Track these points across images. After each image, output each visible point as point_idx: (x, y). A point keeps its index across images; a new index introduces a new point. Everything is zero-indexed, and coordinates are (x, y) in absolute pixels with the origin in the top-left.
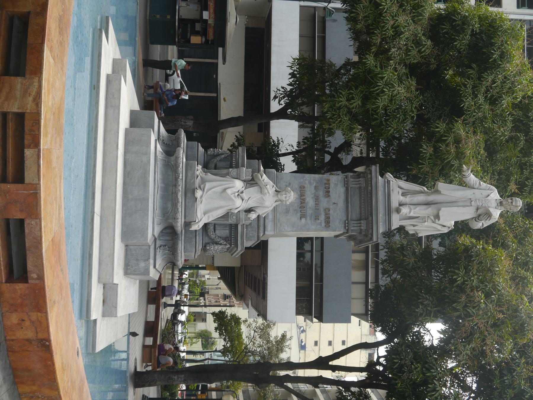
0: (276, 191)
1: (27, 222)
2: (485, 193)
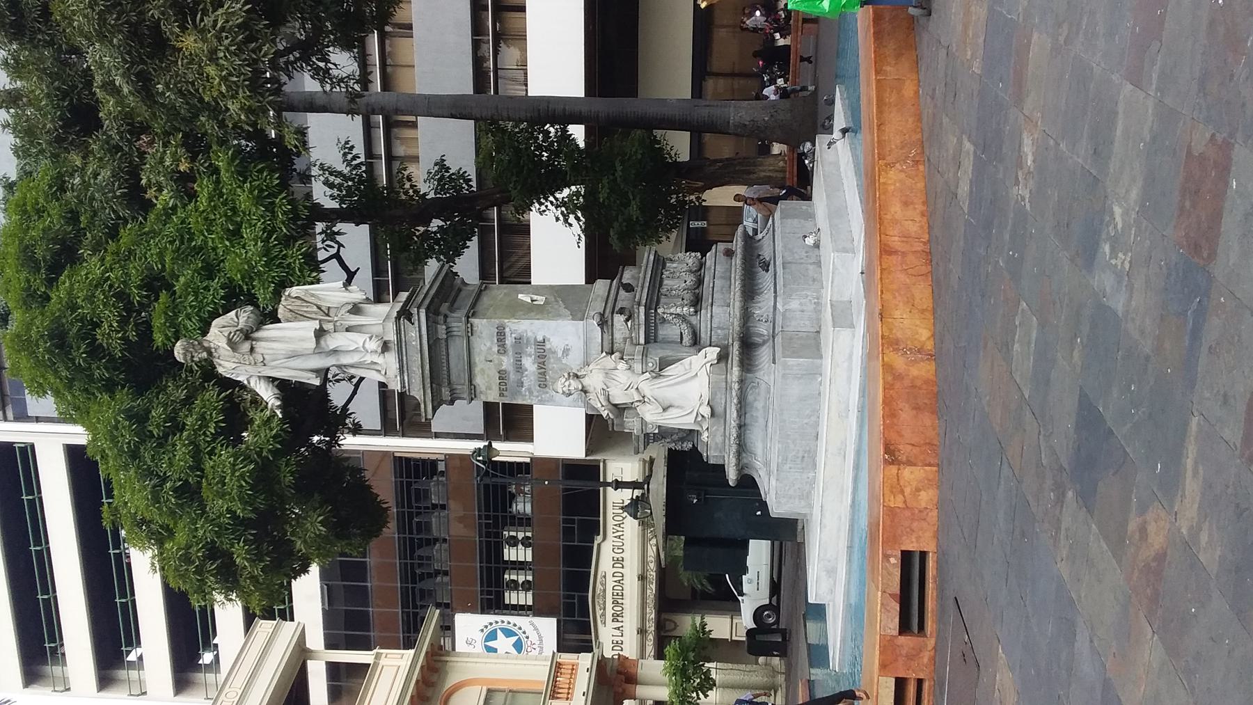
1: (896, 632)
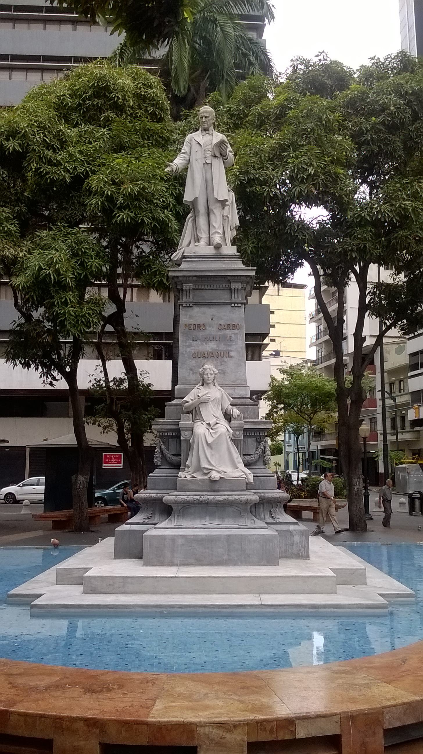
0: (203, 385)
1: (387, 726)
2: (195, 147)
